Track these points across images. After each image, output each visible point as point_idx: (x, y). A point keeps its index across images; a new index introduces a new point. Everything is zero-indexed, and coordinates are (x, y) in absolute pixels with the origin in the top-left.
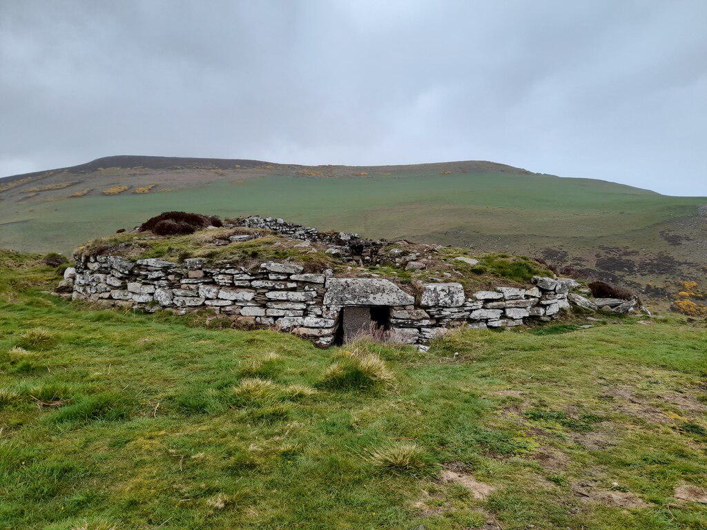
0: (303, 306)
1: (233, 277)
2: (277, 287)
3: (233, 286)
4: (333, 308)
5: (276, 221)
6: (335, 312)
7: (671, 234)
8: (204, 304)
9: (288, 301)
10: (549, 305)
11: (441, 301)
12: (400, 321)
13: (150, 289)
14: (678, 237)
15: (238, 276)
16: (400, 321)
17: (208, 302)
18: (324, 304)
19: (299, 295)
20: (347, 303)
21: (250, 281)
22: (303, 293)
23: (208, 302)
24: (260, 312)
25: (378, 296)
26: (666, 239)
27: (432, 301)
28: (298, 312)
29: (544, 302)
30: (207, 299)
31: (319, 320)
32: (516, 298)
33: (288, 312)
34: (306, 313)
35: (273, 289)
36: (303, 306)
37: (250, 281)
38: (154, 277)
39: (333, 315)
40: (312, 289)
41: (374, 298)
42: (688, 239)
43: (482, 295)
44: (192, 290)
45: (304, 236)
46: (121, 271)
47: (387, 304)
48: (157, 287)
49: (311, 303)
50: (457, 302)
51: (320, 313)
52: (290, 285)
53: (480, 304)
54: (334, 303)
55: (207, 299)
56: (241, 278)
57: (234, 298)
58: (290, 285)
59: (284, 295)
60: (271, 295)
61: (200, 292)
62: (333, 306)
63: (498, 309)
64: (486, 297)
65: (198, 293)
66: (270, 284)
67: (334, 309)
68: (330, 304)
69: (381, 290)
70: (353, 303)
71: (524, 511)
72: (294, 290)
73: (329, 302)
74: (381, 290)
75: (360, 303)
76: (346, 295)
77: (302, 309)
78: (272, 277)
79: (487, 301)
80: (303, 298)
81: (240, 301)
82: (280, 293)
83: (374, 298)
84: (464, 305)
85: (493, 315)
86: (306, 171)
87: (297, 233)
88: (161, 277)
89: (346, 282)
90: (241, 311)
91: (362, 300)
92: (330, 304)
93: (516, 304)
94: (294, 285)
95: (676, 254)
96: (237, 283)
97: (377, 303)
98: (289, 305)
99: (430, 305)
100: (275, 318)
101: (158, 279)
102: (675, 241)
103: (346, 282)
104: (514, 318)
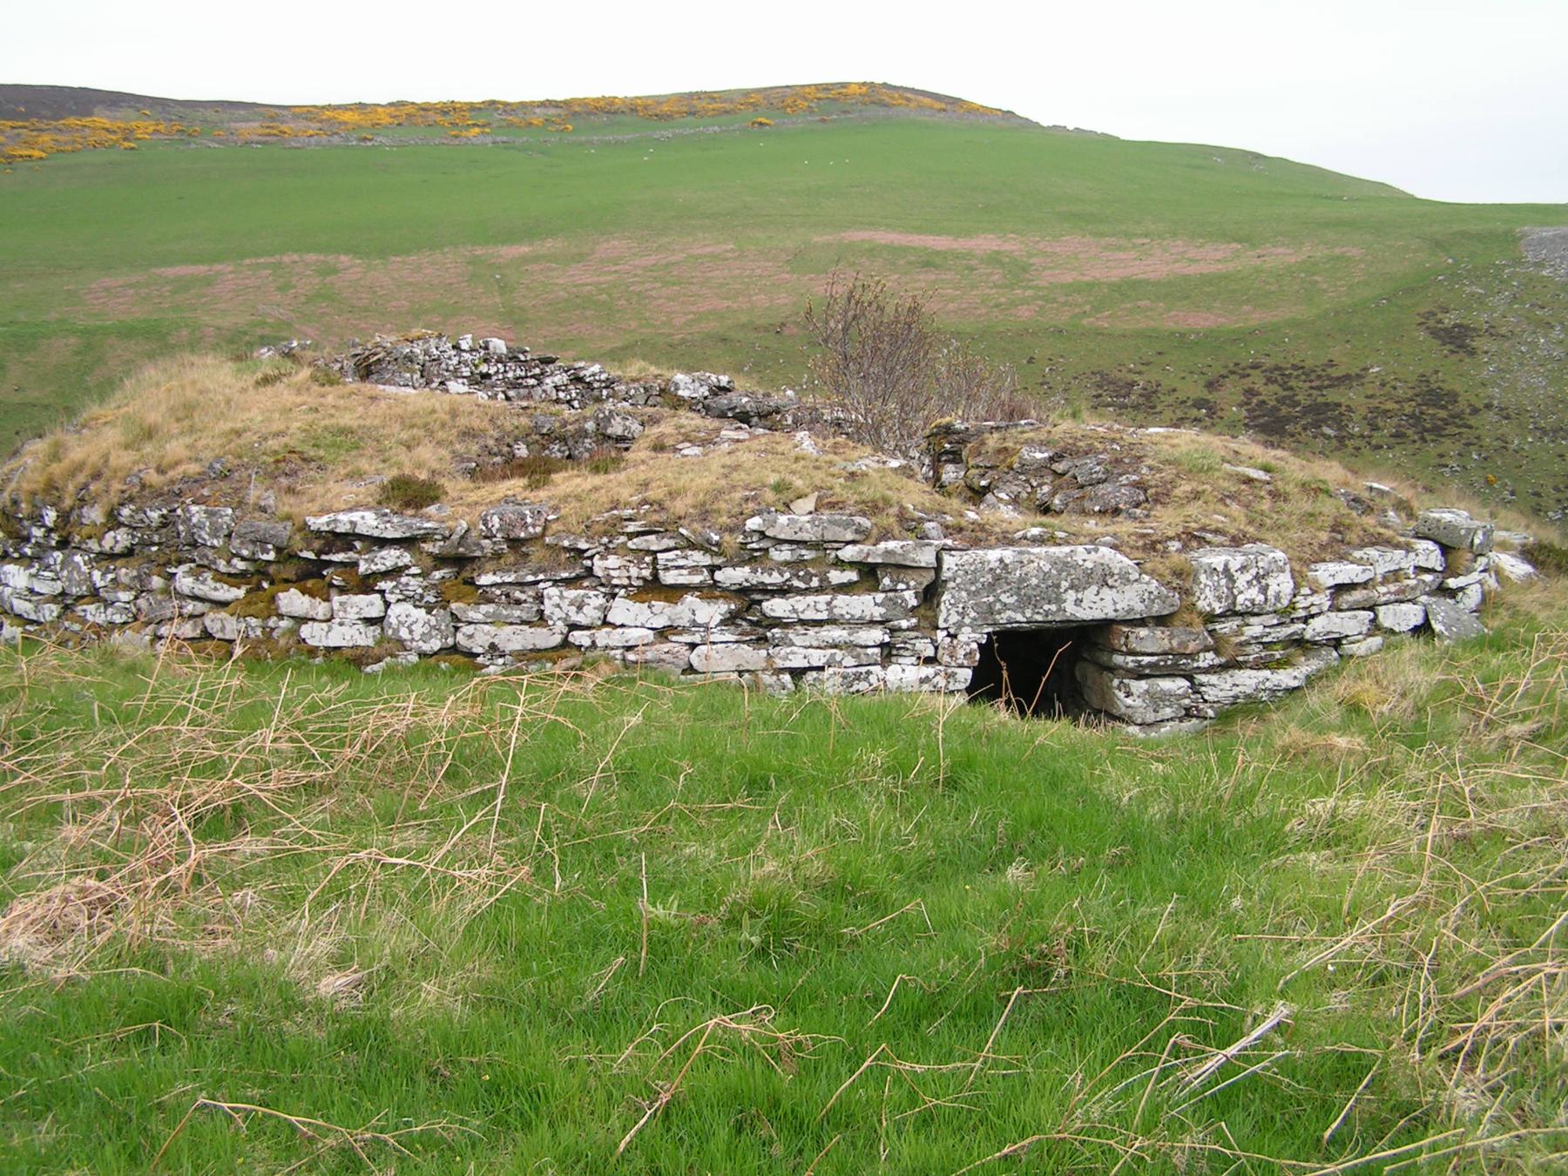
0: (878, 635)
1: (655, 559)
2: (796, 583)
3: (653, 588)
4: (966, 635)
5: (486, 348)
6: (975, 646)
7: (1449, 320)
8: (565, 644)
9: (832, 621)
10: (1462, 589)
11: (1240, 599)
12: (1147, 659)
13: (370, 604)
14: (1467, 328)
15: (671, 555)
16: (1147, 659)
17: (580, 638)
18: (941, 624)
19: (865, 604)
20: (1002, 618)
21: (712, 569)
22: (880, 597)
23: (580, 638)
24: (753, 656)
25: (1089, 594)
26: (1434, 333)
27: (1219, 599)
28: (870, 651)
29: (1452, 583)
30: (574, 627)
31: (928, 671)
32: (1395, 575)
33: (839, 654)
34: (888, 652)
35: (783, 591)
36: (878, 635)
37: (712, 569)
38: (383, 568)
39: (968, 655)
40: (901, 586)
41: (1078, 602)
42: (1492, 332)
43: (1330, 572)
44: (518, 602)
45: (566, 390)
46: (245, 553)
47: (1112, 615)
48: (391, 598)
49: (904, 624)
50: (1278, 597)
51: (930, 652)
52: (836, 577)
53: (1323, 600)
54: (967, 620)
55: (574, 627)
56: (681, 562)
57: (660, 622)
58: (836, 577)
59: (822, 606)
60: (776, 607)
61: (548, 608)
62: (966, 630)
63: (1364, 609)
64: (1342, 579)
65: (541, 612)
66: (775, 578)
67: (971, 639)
68: (960, 625)
69: (1104, 577)
70: (1020, 617)
71: (978, 1064)
72: (845, 588)
73: (954, 618)
74: (1104, 577)
75: (1039, 618)
76: (1004, 598)
77: (882, 645)
78: (783, 554)
79: (1340, 589)
80: (877, 613)
81: (685, 630)
82: (811, 599)
83: (1078, 602)
84: (1293, 606)
85: (1350, 624)
86: (210, 114)
87: (549, 382)
88: (407, 567)
89: (1001, 561)
90: (695, 658)
91: (1046, 607)
92: (960, 625)
93: (1397, 593)
94: (852, 576)
95: (1453, 375)
96: (669, 578)
97: (1084, 614)
98: (837, 634)
99: (1218, 611)
100: (798, 673)
101: (395, 572)
102: (1457, 339)
103: (1001, 561)
104: (1397, 629)
